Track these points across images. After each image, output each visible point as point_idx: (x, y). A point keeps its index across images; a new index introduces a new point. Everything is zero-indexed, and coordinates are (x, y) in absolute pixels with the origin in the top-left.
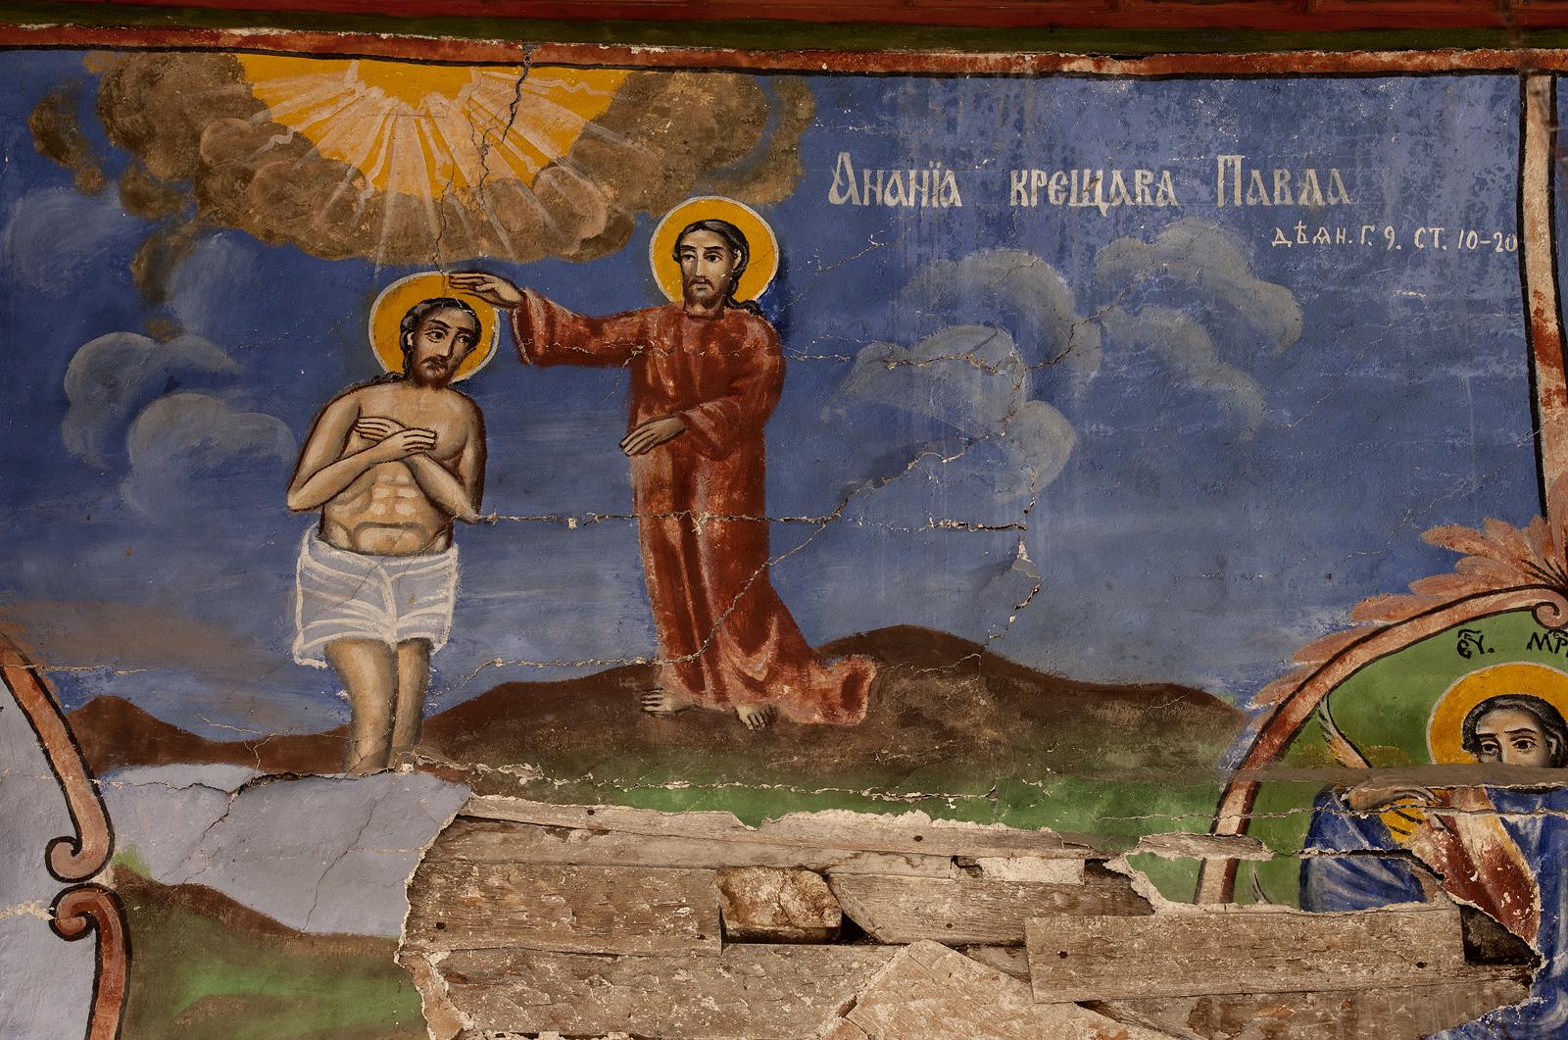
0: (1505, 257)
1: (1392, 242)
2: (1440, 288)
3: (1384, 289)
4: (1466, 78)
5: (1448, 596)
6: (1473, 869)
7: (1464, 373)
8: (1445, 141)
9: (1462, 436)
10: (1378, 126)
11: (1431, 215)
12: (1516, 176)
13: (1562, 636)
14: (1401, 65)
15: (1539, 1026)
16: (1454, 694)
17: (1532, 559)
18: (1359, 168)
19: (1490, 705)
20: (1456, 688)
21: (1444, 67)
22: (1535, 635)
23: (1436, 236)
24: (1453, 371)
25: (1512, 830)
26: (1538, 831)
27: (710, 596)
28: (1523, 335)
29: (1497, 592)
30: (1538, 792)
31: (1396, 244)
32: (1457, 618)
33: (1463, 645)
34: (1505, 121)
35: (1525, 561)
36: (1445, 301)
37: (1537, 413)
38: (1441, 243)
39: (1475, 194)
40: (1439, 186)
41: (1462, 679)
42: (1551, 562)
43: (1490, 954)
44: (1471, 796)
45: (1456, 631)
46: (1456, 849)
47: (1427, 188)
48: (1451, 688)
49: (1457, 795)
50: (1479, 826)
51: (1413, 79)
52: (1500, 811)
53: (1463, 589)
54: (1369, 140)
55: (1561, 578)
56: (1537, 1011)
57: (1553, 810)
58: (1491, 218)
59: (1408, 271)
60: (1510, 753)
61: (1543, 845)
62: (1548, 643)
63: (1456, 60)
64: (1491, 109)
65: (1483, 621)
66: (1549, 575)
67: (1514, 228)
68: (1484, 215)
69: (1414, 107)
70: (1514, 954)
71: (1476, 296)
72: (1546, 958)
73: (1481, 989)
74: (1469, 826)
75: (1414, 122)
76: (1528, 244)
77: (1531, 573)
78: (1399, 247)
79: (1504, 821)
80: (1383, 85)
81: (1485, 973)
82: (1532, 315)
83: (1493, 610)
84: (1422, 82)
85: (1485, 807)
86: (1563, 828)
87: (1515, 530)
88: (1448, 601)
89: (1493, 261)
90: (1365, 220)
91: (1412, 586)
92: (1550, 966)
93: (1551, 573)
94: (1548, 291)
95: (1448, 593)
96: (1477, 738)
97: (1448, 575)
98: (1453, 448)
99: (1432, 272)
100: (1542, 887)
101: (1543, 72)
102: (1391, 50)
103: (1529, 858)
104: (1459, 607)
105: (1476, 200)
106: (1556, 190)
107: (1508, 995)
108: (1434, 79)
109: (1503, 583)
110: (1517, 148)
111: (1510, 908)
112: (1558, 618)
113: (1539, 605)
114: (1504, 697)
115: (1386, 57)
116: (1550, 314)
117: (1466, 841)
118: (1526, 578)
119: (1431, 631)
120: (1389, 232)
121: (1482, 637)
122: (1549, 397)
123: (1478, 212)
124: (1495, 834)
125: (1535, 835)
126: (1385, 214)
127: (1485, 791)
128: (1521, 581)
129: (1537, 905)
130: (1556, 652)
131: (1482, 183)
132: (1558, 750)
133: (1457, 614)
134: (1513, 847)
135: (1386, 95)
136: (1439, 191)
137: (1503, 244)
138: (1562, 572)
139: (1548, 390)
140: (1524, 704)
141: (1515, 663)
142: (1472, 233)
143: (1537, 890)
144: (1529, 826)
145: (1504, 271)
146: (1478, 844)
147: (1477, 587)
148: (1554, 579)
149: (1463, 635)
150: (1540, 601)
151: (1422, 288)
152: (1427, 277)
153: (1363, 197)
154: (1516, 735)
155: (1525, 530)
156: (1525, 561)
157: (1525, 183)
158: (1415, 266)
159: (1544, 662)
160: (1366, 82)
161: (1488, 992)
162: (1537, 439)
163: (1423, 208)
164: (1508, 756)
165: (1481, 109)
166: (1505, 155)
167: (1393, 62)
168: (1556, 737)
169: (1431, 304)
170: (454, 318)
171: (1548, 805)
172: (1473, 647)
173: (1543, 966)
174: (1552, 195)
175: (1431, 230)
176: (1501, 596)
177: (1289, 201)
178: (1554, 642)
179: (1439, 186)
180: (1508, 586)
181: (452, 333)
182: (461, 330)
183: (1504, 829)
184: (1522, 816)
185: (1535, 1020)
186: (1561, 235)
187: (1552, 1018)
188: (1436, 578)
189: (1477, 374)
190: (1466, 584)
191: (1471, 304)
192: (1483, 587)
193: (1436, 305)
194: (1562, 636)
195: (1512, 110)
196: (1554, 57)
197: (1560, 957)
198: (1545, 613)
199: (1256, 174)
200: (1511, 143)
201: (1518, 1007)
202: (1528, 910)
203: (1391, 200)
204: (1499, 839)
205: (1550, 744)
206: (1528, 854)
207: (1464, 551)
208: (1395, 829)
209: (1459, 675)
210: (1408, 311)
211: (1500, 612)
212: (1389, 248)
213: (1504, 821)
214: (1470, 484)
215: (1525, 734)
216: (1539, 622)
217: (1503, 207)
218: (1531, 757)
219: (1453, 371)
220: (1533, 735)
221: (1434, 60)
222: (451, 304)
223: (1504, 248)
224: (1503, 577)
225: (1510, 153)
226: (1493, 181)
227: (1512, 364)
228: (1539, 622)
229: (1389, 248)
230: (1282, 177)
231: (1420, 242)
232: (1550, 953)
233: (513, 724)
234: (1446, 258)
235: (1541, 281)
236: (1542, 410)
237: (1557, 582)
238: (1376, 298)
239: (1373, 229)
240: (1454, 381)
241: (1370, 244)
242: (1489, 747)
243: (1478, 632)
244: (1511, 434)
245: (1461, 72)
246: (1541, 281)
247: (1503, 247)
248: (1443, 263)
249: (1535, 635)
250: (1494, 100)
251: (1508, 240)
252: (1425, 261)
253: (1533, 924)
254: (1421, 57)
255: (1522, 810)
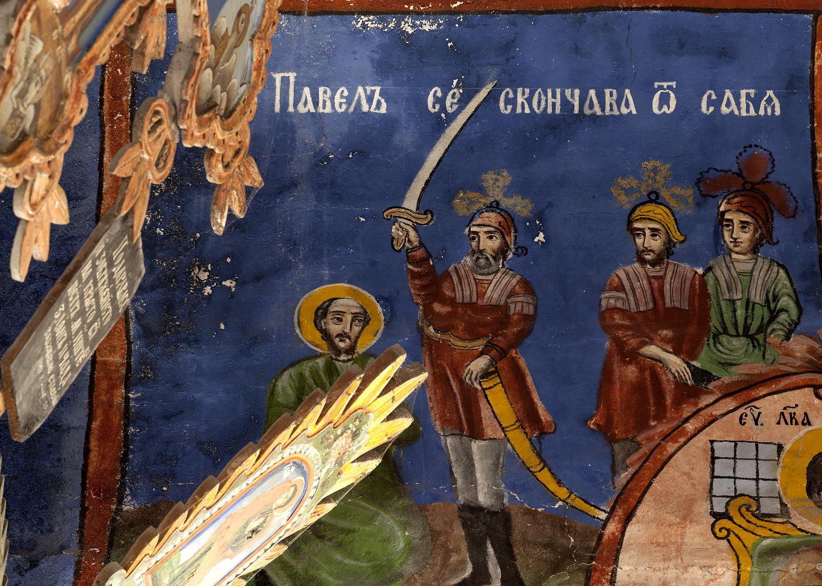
177: (752, 112)
199: (307, 91)
208: (734, 533)
230: (611, 95)
233: (692, 400)
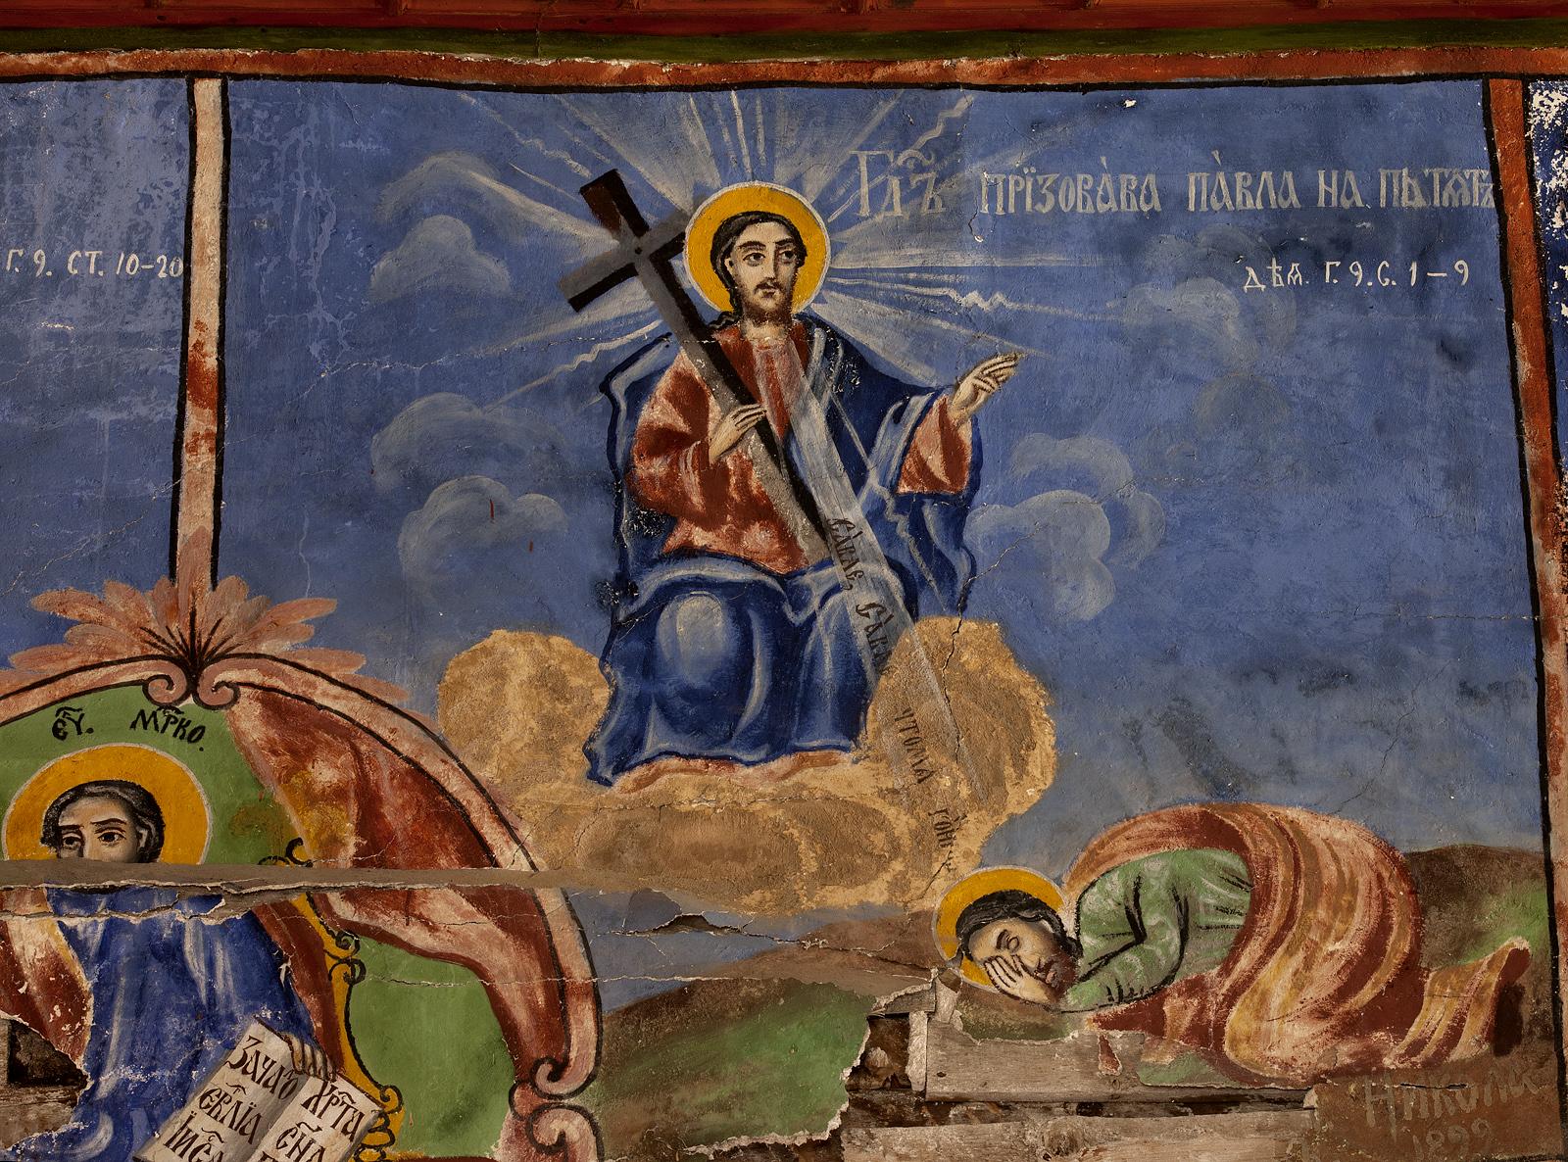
0: (167, 284)
1: (42, 268)
2: (92, 319)
3: (28, 321)
4: (126, 82)
5: (52, 669)
6: (22, 979)
7: (104, 416)
8: (106, 153)
9: (92, 488)
10: (29, 136)
11: (88, 237)
12: (186, 191)
13: (172, 713)
14: (51, 69)
15: (74, 1155)
16: (39, 781)
17: (152, 626)
18: (9, 183)
19: (79, 792)
20: (43, 774)
21: (101, 70)
22: (142, 713)
23: (93, 260)
24: (92, 414)
25: (70, 934)
26: (99, 936)
27: (631, 558)
28: (177, 372)
29: (107, 664)
30: (104, 891)
31: (46, 269)
32: (58, 694)
33: (60, 725)
34: (173, 130)
35: (144, 629)
36: (95, 334)
37: (180, 457)
38: (98, 267)
39: (139, 212)
40: (99, 203)
41: (52, 763)
42: (173, 629)
43: (38, 1074)
44: (28, 897)
45: (55, 708)
46: (5, 958)
47: (85, 206)
48: (38, 774)
49: (13, 897)
50: (33, 931)
51: (67, 83)
52: (57, 913)
53: (70, 662)
54: (21, 153)
55: (181, 647)
56: (75, 1138)
57: (117, 912)
58: (155, 240)
59: (57, 300)
60: (95, 848)
61: (103, 952)
62: (156, 721)
63: (112, 62)
64: (157, 117)
65: (87, 697)
66: (168, 645)
67: (181, 250)
68: (148, 236)
69: (70, 115)
70: (62, 1074)
71: (131, 328)
72: (92, 1079)
73: (25, 1113)
74: (23, 932)
75: (70, 132)
76: (195, 269)
77: (149, 643)
78: (49, 274)
79: (61, 925)
80: (34, 91)
81: (30, 1096)
82: (190, 348)
83: (100, 685)
84: (78, 87)
85: (41, 910)
86: (126, 932)
87: (139, 595)
88: (51, 675)
89: (154, 287)
90: (13, 244)
91: (13, 659)
92: (95, 1087)
93: (172, 642)
94: (212, 322)
95: (52, 666)
96: (58, 830)
97: (55, 646)
98: (80, 501)
99: (84, 302)
100: (97, 998)
101: (211, 75)
102: (41, 51)
103: (86, 967)
104: (63, 681)
105: (140, 219)
106: (230, 207)
107: (54, 1120)
108: (90, 83)
109: (116, 653)
110: (187, 159)
111: (59, 1022)
112: (171, 692)
113: (151, 679)
114: (97, 783)
115: (34, 59)
116: (211, 348)
117: (17, 948)
118: (142, 648)
119: (26, 710)
120: (39, 256)
121: (82, 716)
122: (195, 442)
123: (142, 232)
124: (51, 940)
125: (95, 940)
126: (36, 235)
127: (45, 891)
128: (137, 651)
129: (89, 1019)
130: (163, 731)
131: (147, 200)
132: (148, 842)
133: (58, 690)
134: (69, 954)
135: (38, 102)
136: (98, 210)
137: (167, 268)
138: (184, 641)
139: (195, 435)
140: (117, 791)
141: (114, 745)
142: (134, 257)
143: (91, 1002)
144: (90, 930)
145: (165, 299)
146: (30, 951)
147: (85, 658)
148: (173, 649)
149: (62, 713)
150: (153, 674)
151: (71, 319)
152: (77, 307)
153: (12, 218)
154: (103, 826)
155: (149, 593)
156: (144, 629)
157: (196, 200)
158: (65, 296)
159: (146, 743)
160: (13, 87)
161: (32, 1116)
162: (177, 490)
163: (80, 227)
164: (90, 851)
165: (146, 117)
166: (174, 168)
167: (42, 64)
168: (148, 828)
169: (78, 338)
170: (768, 234)
171: (112, 906)
172: (70, 727)
173: (88, 1087)
174: (224, 213)
175: (87, 254)
176: (112, 669)
178: (161, 719)
179: (99, 203)
180: (121, 657)
181: (771, 249)
182: (780, 243)
183: (61, 933)
184: (83, 919)
185: (72, 1148)
186: (232, 258)
187: (91, 1145)
188: (40, 650)
189: (119, 416)
190: (74, 656)
191: (124, 338)
192: (93, 659)
193: (84, 338)
194: (172, 713)
195: (181, 117)
196: (223, 58)
197: (107, 1077)
198: (158, 689)
200: (180, 154)
201: (55, 1134)
202: (78, 1024)
203: (43, 219)
204: (54, 945)
205: (139, 836)
206: (86, 962)
207: (77, 618)
209: (49, 760)
210: (51, 346)
211: (108, 687)
212: (38, 274)
213: (61, 925)
214: (93, 542)
215: (113, 824)
216: (149, 698)
217: (170, 227)
218: (117, 851)
219: (92, 414)
220: (122, 826)
221: (88, 62)
222: (766, 217)
223: (168, 273)
224: (118, 647)
225: (180, 166)
226: (159, 197)
227: (159, 405)
228: (149, 698)
229: (38, 274)
231: (74, 267)
232: (97, 1072)
234: (101, 285)
235: (206, 310)
236: (186, 457)
237: (177, 652)
238: (17, 331)
239: (21, 253)
240: (93, 424)
241: (17, 270)
242: (70, 841)
243: (78, 710)
244: (148, 485)
245: (119, 76)
246: (206, 310)
247: (167, 271)
248: (98, 291)
249: (142, 713)
250: (160, 107)
251: (173, 264)
252: (77, 289)
253: (82, 1040)
254: (74, 60)
255: (82, 912)
